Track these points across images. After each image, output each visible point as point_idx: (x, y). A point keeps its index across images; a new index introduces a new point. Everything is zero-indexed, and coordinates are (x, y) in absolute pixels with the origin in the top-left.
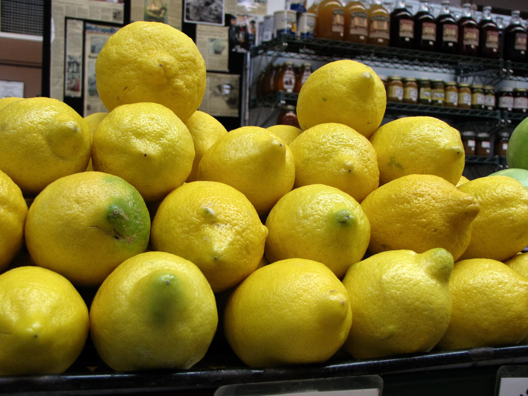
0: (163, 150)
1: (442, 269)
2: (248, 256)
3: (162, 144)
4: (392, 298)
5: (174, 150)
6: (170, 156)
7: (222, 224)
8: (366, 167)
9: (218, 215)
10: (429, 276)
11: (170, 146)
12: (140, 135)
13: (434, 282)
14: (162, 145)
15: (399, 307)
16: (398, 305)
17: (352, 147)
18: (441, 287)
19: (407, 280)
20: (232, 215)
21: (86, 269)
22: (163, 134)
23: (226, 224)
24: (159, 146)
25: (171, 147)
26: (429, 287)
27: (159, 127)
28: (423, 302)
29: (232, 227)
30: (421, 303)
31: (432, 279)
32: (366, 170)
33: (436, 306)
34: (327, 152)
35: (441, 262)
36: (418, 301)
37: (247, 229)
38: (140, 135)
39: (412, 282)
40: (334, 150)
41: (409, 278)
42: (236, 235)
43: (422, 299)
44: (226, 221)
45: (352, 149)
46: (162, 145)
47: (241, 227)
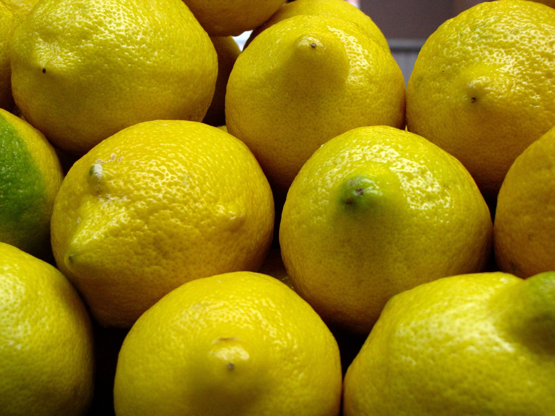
0: (83, 61)
1: (536, 320)
2: (164, 261)
3: (82, 51)
4: (401, 373)
5: (108, 62)
6: (99, 72)
7: (113, 196)
8: (538, 91)
9: (110, 178)
10: (503, 333)
11: (98, 54)
12: (50, 36)
13: (508, 347)
14: (81, 52)
15: (411, 397)
16: (411, 392)
17: (508, 48)
18: (530, 363)
19: (440, 337)
20: (138, 180)
21: (349, 298)
22: (88, 33)
23: (121, 197)
24: (76, 54)
25: (99, 56)
26: (491, 359)
27: (84, 20)
28: (465, 392)
29: (130, 203)
30: (460, 394)
31: (507, 340)
32: (537, 97)
33: (501, 405)
34: (450, 62)
35: (535, 304)
36: (453, 387)
37: (165, 208)
38: (50, 36)
39: (450, 343)
40: (466, 58)
41: (447, 335)
42: (133, 217)
43: (466, 385)
44: (123, 191)
45: (508, 53)
46: (81, 52)
47: (149, 203)
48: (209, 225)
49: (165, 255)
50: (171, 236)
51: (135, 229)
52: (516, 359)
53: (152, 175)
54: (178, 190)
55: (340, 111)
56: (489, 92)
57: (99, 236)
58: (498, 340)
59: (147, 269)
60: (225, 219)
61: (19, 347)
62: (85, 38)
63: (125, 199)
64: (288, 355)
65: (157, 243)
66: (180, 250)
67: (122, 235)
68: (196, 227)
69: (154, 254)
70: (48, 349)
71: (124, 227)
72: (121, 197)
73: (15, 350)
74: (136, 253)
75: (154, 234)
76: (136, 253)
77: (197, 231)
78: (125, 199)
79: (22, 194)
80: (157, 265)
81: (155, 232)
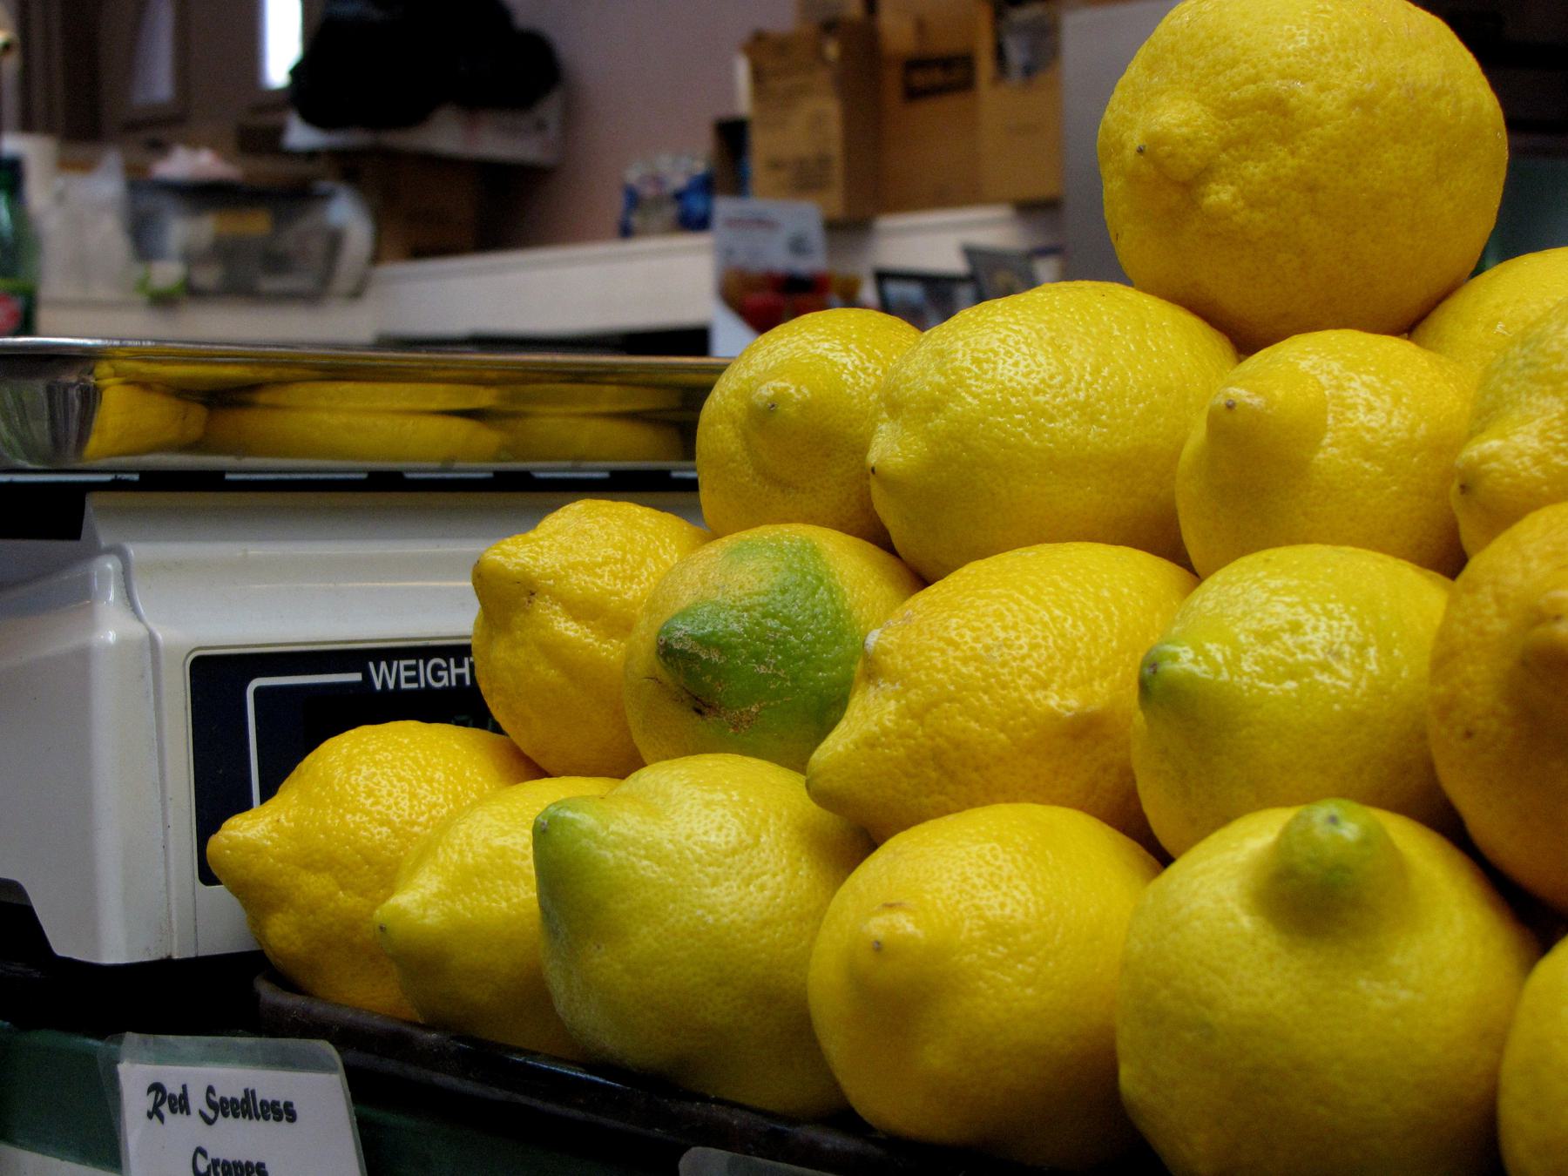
2: (951, 788)
13: (1246, 922)
23: (893, 683)
37: (951, 700)
48: (1026, 728)
49: (952, 776)
50: (958, 746)
51: (904, 735)
52: (1254, 943)
53: (942, 644)
54: (977, 669)
55: (1305, 514)
56: (1488, 473)
57: (846, 747)
58: (1237, 910)
59: (925, 801)
60: (1054, 716)
61: (710, 919)
62: (937, 410)
63: (898, 687)
64: (998, 932)
65: (937, 757)
66: (977, 769)
67: (882, 745)
68: (1002, 731)
69: (934, 775)
70: (766, 924)
71: (885, 732)
72: (893, 683)
73: (705, 923)
74: (907, 775)
75: (929, 743)
76: (907, 775)
77: (1002, 736)
78: (898, 687)
79: (824, 679)
80: (941, 793)
81: (932, 739)
